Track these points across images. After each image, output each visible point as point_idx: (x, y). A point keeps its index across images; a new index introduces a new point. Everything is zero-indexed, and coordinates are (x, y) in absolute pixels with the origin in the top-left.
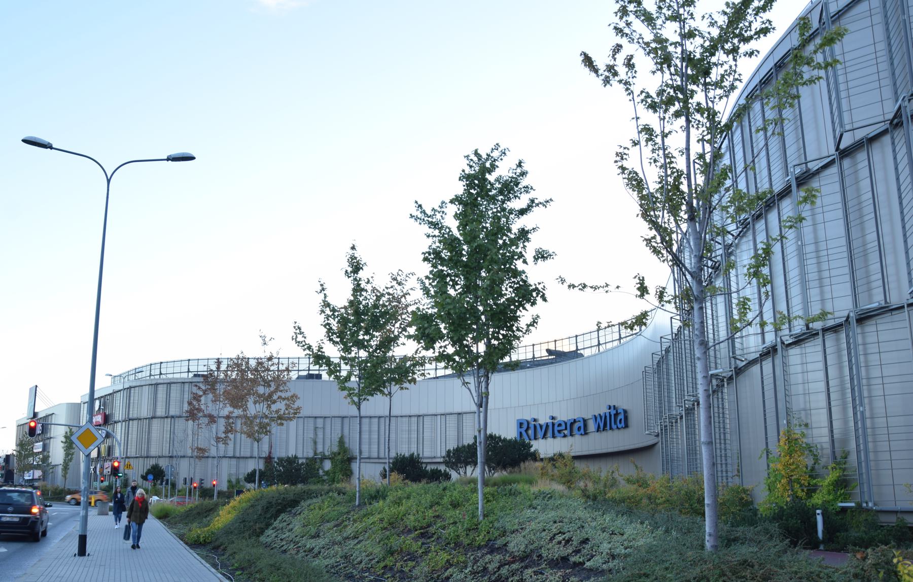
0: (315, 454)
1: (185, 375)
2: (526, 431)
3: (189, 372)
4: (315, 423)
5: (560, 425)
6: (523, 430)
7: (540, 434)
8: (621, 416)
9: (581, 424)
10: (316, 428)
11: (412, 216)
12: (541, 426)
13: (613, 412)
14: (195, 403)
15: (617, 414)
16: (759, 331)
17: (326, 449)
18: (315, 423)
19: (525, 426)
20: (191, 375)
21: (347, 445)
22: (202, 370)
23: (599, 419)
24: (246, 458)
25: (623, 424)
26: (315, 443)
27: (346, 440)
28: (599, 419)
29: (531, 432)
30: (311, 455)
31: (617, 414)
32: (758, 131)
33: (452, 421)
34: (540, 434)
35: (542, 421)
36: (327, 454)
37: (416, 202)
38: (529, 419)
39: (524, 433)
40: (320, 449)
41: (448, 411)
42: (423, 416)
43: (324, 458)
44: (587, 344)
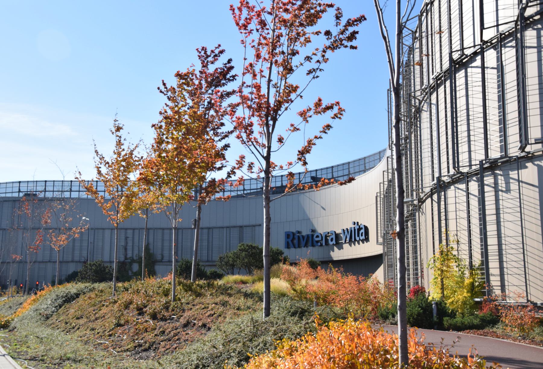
0: (126, 258)
1: (16, 195)
2: (292, 241)
3: (19, 191)
4: (126, 233)
5: (317, 237)
6: (290, 240)
7: (303, 243)
8: (363, 231)
9: (334, 236)
10: (126, 238)
11: (219, 45)
12: (303, 237)
13: (357, 227)
14: (177, 104)
15: (360, 229)
16: (424, 189)
17: (135, 255)
18: (126, 233)
19: (291, 237)
20: (21, 195)
21: (151, 251)
22: (31, 187)
23: (346, 232)
24: (68, 262)
25: (363, 237)
26: (126, 249)
27: (151, 247)
28: (346, 232)
29: (296, 241)
30: (122, 259)
31: (360, 229)
32: (424, 32)
33: (235, 233)
34: (303, 243)
35: (304, 234)
36: (135, 258)
37: (163, 81)
38: (294, 231)
39: (290, 242)
40: (129, 255)
41: (232, 225)
42: (212, 228)
43: (133, 261)
44: (340, 173)
